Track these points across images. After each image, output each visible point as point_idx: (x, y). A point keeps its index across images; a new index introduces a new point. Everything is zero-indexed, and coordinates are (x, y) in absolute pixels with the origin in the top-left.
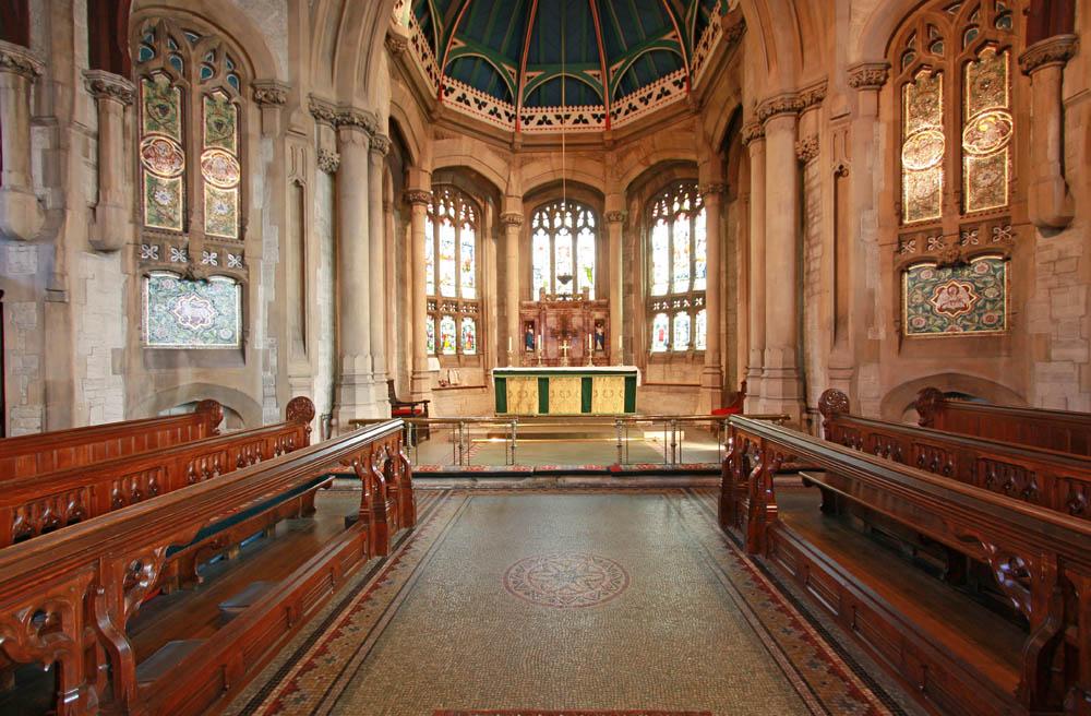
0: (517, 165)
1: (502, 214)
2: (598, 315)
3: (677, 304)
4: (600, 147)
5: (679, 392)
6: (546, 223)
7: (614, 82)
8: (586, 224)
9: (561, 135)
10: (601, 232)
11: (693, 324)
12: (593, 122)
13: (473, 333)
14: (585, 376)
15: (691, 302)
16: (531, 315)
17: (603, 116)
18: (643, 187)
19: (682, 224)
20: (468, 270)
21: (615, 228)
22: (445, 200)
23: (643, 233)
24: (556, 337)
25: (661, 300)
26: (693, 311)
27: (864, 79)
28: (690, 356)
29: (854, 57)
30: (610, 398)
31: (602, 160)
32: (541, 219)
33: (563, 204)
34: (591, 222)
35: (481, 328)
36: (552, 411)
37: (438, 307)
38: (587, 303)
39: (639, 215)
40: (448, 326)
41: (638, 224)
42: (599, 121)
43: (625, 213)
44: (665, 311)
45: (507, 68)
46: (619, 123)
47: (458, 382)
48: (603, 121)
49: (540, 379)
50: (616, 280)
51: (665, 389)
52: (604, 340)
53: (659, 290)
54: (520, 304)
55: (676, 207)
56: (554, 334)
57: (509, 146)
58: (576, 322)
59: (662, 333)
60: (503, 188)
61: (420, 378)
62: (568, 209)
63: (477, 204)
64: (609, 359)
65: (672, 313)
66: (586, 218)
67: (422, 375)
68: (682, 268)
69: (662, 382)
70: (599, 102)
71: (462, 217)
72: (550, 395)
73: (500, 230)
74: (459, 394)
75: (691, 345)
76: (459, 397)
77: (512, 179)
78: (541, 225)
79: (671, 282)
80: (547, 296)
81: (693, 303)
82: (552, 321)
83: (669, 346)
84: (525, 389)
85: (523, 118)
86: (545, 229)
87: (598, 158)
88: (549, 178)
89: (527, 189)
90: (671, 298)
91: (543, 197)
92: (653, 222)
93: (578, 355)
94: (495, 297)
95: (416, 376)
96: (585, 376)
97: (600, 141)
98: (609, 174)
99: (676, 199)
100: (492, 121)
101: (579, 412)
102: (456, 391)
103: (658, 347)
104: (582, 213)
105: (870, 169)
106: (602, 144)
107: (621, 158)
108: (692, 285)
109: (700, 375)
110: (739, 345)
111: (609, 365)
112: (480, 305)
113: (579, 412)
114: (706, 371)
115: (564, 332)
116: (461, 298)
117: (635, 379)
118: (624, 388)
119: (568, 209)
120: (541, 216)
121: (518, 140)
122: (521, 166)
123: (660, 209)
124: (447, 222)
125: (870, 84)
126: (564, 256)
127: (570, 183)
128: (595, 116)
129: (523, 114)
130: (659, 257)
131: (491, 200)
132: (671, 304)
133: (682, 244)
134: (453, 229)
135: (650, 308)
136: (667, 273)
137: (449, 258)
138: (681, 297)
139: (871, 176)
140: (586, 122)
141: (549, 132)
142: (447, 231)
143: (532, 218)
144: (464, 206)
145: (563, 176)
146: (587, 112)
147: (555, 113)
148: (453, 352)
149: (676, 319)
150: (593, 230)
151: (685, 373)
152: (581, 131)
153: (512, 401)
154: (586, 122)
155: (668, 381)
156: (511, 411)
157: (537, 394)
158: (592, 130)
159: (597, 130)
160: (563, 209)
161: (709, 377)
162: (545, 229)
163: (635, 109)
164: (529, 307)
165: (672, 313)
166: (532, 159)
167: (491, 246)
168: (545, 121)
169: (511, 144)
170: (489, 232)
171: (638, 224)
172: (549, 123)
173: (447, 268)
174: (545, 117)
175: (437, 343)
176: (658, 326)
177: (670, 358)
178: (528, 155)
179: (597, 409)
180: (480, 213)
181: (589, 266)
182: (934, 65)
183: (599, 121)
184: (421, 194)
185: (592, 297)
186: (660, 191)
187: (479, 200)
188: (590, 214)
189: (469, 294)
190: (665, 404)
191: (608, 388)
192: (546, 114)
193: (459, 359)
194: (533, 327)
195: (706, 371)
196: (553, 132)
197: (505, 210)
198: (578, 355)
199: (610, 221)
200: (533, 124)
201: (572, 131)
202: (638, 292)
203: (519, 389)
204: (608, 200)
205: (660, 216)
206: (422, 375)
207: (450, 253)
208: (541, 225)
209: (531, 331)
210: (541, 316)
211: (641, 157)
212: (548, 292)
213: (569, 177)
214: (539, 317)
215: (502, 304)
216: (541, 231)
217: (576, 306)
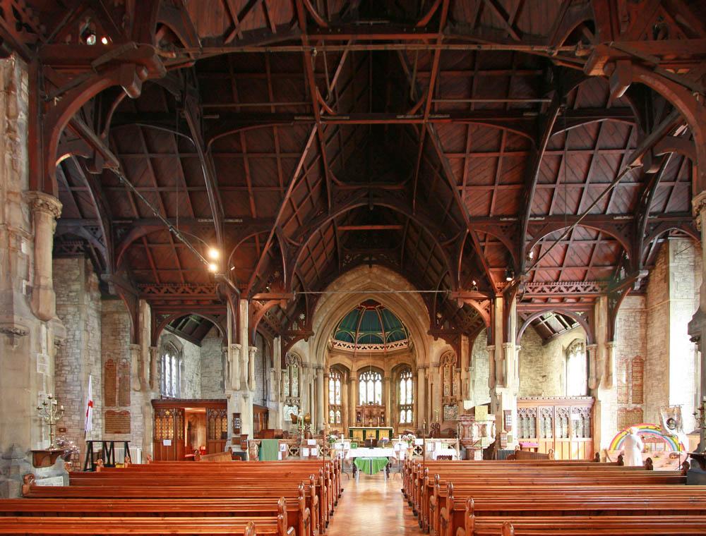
2: (382, 410)
6: (364, 378)
8: (378, 379)
10: (383, 381)
16: (359, 410)
21: (388, 382)
25: (403, 406)
46: (389, 350)
56: (367, 417)
57: (353, 356)
58: (375, 413)
60: (350, 369)
65: (406, 410)
82: (366, 412)
83: (405, 421)
92: (401, 380)
115: (370, 416)
135: (400, 408)
143: (359, 377)
150: (381, 381)
165: (406, 410)
167: (346, 387)
180: (342, 376)
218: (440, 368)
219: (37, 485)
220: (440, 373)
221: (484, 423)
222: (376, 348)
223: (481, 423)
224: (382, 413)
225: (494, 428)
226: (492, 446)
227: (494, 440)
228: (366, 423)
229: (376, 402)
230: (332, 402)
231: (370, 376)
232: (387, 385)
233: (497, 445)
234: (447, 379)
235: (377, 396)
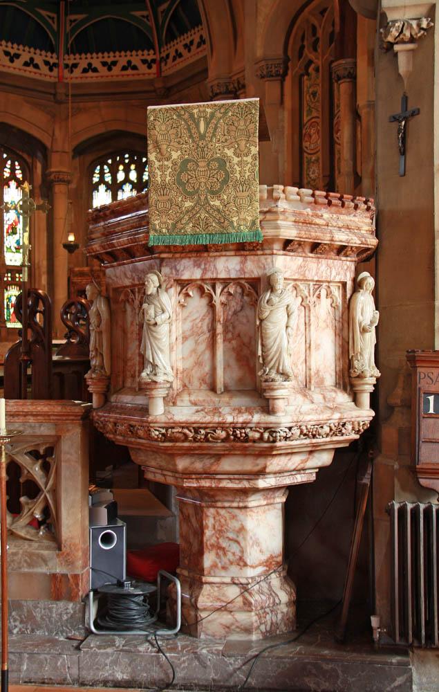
1: (47, 171)
6: (108, 178)
7: (164, 22)
12: (143, 68)
17: (154, 61)
27: (265, 73)
29: (259, 53)
32: (102, 173)
33: (127, 156)
42: (150, 67)
45: (44, 13)
46: (170, 68)
48: (154, 66)
54: (71, 271)
57: (48, 96)
60: (48, 144)
70: (150, 46)
77: (57, 133)
78: (102, 181)
85: (67, 66)
86: (106, 184)
89: (75, 143)
94: (45, 263)
97: (152, 88)
100: (30, 72)
105: (277, 151)
106: (155, 91)
121: (61, 90)
125: (272, 76)
128: (144, 62)
129: (66, 62)
139: (277, 158)
140: (135, 68)
141: (94, 80)
146: (136, 58)
147: (101, 59)
152: (131, 78)
154: (135, 68)
158: (141, 77)
159: (147, 77)
160: (127, 161)
162: (106, 184)
163: (180, 56)
168: (90, 68)
169: (55, 95)
172: (95, 70)
174: (90, 65)
178: (81, 105)
182: (301, 72)
183: (150, 67)
187: (25, 156)
192: (92, 61)
196: (100, 80)
197: (51, 168)
200: (77, 72)
201: (120, 79)
208: (102, 181)
216: (102, 188)
220: (288, 102)
221: (252, 268)
222: (129, 66)
223: (227, 266)
225: (366, 309)
226: (356, 456)
227: (365, 414)
231: (127, 171)
233: (387, 460)
234: (313, 115)
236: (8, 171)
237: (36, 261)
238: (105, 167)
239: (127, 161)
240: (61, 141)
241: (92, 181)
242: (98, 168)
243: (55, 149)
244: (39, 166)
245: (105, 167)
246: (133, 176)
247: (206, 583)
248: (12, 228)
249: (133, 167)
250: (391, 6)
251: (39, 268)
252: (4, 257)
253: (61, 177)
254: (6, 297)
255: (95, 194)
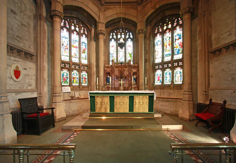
0: (103, 10)
2: (134, 70)
3: (166, 66)
4: (135, 4)
5: (168, 101)
6: (115, 37)
8: (129, 37)
9: (121, 17)
10: (135, 41)
11: (173, 73)
13: (86, 77)
14: (131, 95)
15: (172, 65)
16: (109, 70)
18: (152, 21)
19: (168, 35)
20: (84, 53)
21: (141, 37)
22: (74, 24)
23: (152, 39)
24: (118, 79)
25: (159, 64)
26: (173, 68)
28: (172, 86)
30: (141, 106)
31: (136, 9)
34: (131, 37)
35: (90, 76)
36: (116, 111)
37: (69, 66)
38: (130, 66)
39: (150, 32)
40: (75, 74)
41: (150, 36)
43: (145, 30)
44: (160, 69)
47: (79, 96)
49: (110, 97)
50: (142, 56)
51: (161, 99)
52: (137, 80)
53: (158, 60)
54: (104, 66)
55: (165, 28)
56: (117, 78)
58: (126, 73)
59: (159, 78)
60: (98, 20)
61: (56, 96)
62: (123, 32)
63: (88, 27)
64: (138, 87)
65: (163, 70)
66: (129, 35)
67: (57, 95)
68: (168, 51)
69: (160, 97)
71: (82, 32)
72: (115, 104)
73: (97, 39)
74: (79, 101)
75: (172, 82)
76: (79, 103)
77: (101, 16)
78: (113, 38)
79: (163, 57)
80: (115, 63)
81: (163, 66)
82: (117, 72)
83: (163, 82)
84: (104, 101)
86: (114, 39)
87: (134, 8)
88: (115, 17)
90: (163, 63)
91: (114, 26)
92: (155, 35)
93: (126, 86)
94: (95, 63)
95: (54, 95)
96: (131, 95)
98: (139, 14)
99: (165, 25)
101: (128, 111)
102: (78, 100)
103: (158, 83)
104: (128, 33)
107: (144, 7)
108: (172, 57)
109: (184, 95)
110: (199, 82)
111: (138, 90)
112: (89, 66)
113: (128, 111)
114: (185, 93)
115: (121, 76)
116: (81, 63)
117: (153, 97)
118: (148, 101)
119: (123, 32)
120: (113, 34)
122: (105, 11)
123: (158, 29)
124: (75, 33)
126: (121, 51)
127: (125, 20)
130: (158, 48)
131: (93, 26)
132: (163, 66)
133: (167, 42)
134: (78, 36)
135: (154, 67)
136: (161, 54)
137: (76, 47)
138: (168, 63)
142: (75, 36)
143: (110, 35)
144: (83, 28)
145: (122, 16)
148: (77, 84)
149: (175, 71)
150: (132, 40)
151: (170, 93)
153: (98, 106)
155: (162, 96)
156: (97, 111)
157: (109, 104)
161: (187, 96)
162: (114, 39)
164: (108, 67)
165: (163, 70)
166: (109, 8)
167: (94, 44)
170: (92, 38)
171: (150, 36)
173: (75, 51)
175: (70, 80)
176: (157, 74)
177: (163, 87)
178: (107, 6)
179: (136, 110)
180: (89, 31)
181: (131, 53)
184: (57, 12)
185: (132, 63)
186: (159, 22)
187: (88, 26)
188: (131, 34)
189: (85, 62)
190: (161, 105)
191: (141, 101)
193: (80, 88)
194: (109, 75)
195: (185, 93)
197: (98, 28)
198: (126, 86)
199: (139, 33)
202: (150, 61)
203: (101, 101)
204: (139, 25)
205: (158, 32)
206: (57, 95)
207: (72, 44)
208: (113, 38)
209: (109, 76)
210: (113, 71)
211: (152, 6)
212: (115, 61)
213: (123, 17)
214: (112, 71)
215: (98, 66)
216: (113, 40)
217: (126, 67)
218: (205, 17)
219: (161, 70)
224: (134, 74)
228: (117, 84)
229: (127, 61)
230: (65, 58)
231: (121, 35)
232: (140, 39)
235: (128, 55)
236: (82, 31)
237: (92, 63)
238: (114, 33)
239: (121, 32)
240: (103, 17)
241: (110, 38)
242: (112, 34)
243: (100, 22)
244: (93, 30)
245: (114, 33)
246: (123, 36)
247: (172, 82)
248: (84, 51)
249: (123, 34)
250: (199, 2)
251: (93, 65)
252: (96, 45)
253: (102, 32)
254: (82, 75)
255: (111, 42)
